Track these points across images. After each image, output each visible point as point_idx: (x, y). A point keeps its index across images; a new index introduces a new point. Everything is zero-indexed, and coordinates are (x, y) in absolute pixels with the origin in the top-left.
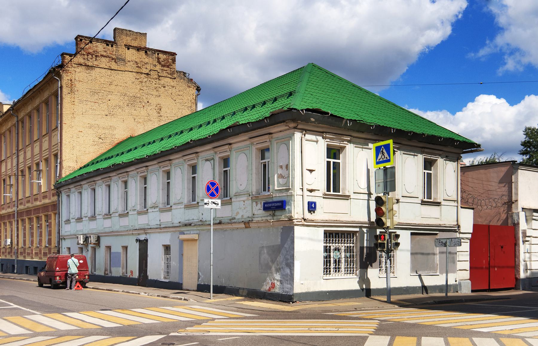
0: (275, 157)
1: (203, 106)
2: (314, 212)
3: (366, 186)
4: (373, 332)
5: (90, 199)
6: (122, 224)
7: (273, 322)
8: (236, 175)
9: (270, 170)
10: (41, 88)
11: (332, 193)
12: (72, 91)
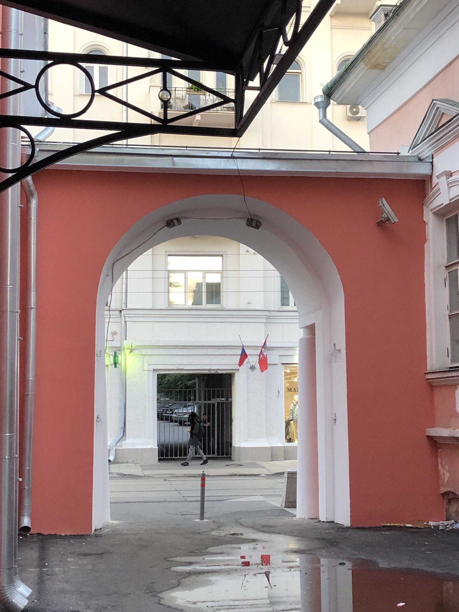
0: (447, 28)
1: (376, 26)
2: (248, 225)
3: (129, 102)
4: (180, 581)
5: (177, 372)
6: (216, 263)
8: (123, 145)
9: (253, 324)
10: (263, 606)
11: (220, 456)
12: (442, 204)
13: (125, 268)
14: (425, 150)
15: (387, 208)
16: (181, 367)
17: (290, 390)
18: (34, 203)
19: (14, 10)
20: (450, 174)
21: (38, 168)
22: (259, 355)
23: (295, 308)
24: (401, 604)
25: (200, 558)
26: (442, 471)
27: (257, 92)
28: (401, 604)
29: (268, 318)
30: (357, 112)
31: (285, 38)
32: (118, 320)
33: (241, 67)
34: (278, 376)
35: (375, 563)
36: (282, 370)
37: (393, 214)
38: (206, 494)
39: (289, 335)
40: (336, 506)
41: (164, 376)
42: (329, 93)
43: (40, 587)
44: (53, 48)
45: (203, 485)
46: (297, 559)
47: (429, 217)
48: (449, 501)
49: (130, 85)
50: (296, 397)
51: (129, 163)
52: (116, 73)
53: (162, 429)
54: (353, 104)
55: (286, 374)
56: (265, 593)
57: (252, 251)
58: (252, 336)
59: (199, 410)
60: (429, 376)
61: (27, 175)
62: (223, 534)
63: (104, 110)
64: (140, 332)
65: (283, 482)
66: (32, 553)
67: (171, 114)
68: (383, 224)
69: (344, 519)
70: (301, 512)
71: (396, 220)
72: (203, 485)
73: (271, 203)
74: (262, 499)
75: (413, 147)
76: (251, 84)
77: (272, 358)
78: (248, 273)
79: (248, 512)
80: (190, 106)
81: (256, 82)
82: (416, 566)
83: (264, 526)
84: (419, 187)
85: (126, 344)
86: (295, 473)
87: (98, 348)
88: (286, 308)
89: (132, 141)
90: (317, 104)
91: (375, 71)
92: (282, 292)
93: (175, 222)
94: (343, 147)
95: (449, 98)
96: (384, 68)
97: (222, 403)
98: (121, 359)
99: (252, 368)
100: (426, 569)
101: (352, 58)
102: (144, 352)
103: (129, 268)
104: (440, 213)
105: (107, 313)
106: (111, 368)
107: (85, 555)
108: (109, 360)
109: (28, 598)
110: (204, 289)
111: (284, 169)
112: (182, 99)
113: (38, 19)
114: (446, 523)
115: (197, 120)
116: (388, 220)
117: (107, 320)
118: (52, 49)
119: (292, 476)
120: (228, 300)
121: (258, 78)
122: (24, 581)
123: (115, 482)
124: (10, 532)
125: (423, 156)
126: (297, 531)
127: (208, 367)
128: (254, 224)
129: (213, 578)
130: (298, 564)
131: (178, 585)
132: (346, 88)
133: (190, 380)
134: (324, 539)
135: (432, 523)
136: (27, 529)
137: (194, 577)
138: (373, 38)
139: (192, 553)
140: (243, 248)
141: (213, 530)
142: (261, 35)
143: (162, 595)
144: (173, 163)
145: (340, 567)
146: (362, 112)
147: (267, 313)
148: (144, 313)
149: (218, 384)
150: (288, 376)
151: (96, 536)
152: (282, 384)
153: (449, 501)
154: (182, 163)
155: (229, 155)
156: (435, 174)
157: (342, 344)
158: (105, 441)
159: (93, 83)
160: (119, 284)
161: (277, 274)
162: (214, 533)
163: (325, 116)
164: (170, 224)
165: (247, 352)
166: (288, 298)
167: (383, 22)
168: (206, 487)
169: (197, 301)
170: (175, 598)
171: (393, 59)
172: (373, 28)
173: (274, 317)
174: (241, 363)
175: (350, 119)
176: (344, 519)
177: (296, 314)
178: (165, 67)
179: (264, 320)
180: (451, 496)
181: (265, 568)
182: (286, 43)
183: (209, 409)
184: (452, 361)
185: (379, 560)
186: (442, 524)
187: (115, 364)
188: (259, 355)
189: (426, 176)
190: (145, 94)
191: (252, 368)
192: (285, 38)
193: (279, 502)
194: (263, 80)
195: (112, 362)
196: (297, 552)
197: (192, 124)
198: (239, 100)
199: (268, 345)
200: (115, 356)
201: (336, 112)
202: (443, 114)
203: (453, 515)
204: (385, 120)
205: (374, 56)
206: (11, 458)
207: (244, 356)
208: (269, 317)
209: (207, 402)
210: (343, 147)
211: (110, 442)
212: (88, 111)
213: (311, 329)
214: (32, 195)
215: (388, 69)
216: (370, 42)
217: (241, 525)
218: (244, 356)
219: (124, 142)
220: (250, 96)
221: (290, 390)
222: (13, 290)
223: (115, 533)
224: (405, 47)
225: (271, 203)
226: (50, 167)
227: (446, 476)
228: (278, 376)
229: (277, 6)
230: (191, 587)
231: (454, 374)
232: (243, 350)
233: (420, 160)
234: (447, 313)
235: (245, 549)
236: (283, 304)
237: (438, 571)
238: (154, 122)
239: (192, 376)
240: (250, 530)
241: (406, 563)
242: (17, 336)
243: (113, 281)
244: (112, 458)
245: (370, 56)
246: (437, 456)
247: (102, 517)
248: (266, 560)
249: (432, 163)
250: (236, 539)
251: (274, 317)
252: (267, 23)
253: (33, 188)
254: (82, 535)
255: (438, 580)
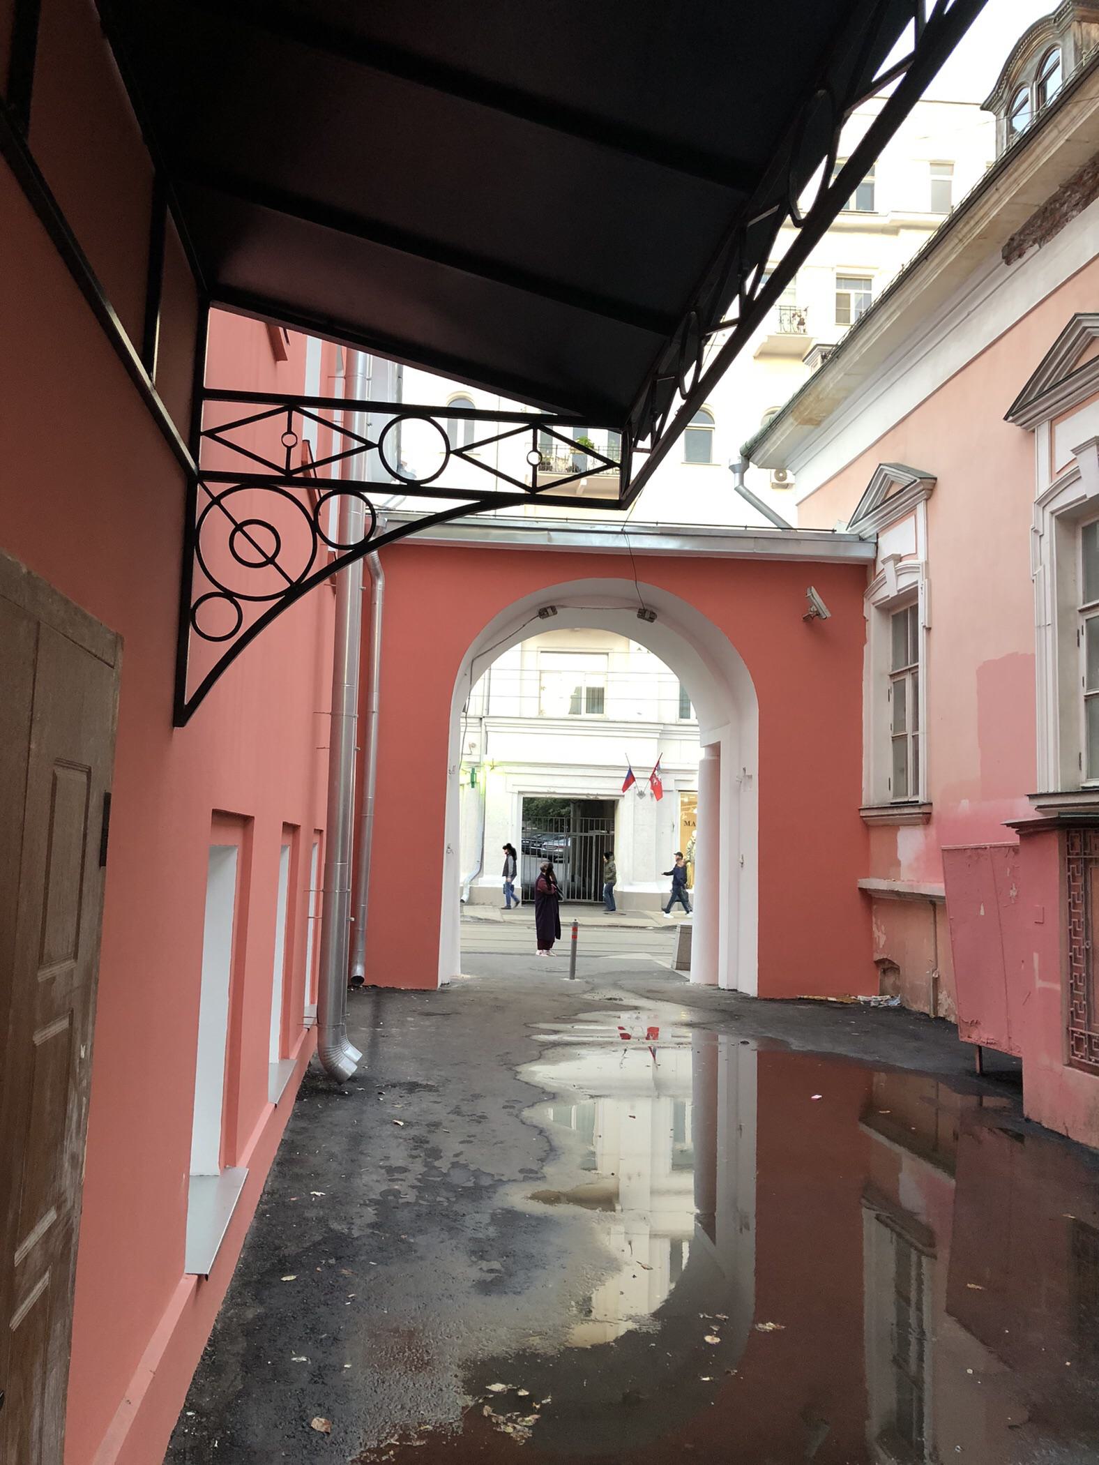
4: (542, 1052)
7: (1019, 166)
13: (487, 665)
14: (867, 528)
15: (817, 599)
16: (552, 790)
17: (688, 823)
18: (380, 584)
19: (361, 354)
20: (899, 559)
21: (387, 542)
22: (651, 779)
23: (696, 722)
24: (817, 1097)
25: (569, 1026)
26: (877, 933)
27: (648, 455)
28: (817, 1097)
29: (663, 733)
30: (784, 478)
31: (682, 390)
32: (478, 729)
33: (630, 423)
34: (673, 805)
35: (786, 1044)
36: (678, 799)
37: (823, 607)
38: (578, 947)
39: (687, 755)
40: (740, 971)
41: (532, 799)
42: (748, 454)
43: (372, 1050)
44: (408, 399)
45: (575, 937)
46: (689, 1034)
47: (870, 612)
48: (884, 972)
49: (500, 441)
50: (695, 833)
51: (495, 537)
52: (484, 429)
53: (527, 865)
54: (780, 467)
55: (682, 803)
56: (648, 1074)
57: (644, 649)
58: (642, 754)
59: (572, 842)
60: (863, 814)
61: (372, 549)
62: (597, 998)
63: (461, 476)
64: (504, 745)
65: (675, 937)
66: (363, 1010)
67: (544, 478)
68: (811, 620)
69: (750, 987)
70: (696, 976)
71: (828, 614)
72: (575, 937)
73: (678, 591)
74: (648, 957)
75: (853, 523)
76: (641, 444)
77: (668, 783)
78: (638, 676)
79: (629, 972)
80: (574, 468)
81: (646, 443)
82: (841, 1050)
83: (649, 991)
84: (859, 574)
85: (487, 760)
86: (690, 928)
87: (451, 764)
88: (685, 721)
89: (500, 511)
90: (732, 468)
91: (808, 427)
92: (682, 701)
93: (549, 611)
94: (765, 522)
95: (900, 462)
96: (818, 423)
97: (602, 837)
98: (479, 777)
99: (641, 794)
100: (852, 1055)
101: (779, 410)
102: (508, 769)
103: (493, 666)
104: (886, 608)
105: (463, 720)
106: (468, 788)
107: (428, 1014)
108: (464, 778)
109: (357, 1063)
110: (584, 695)
111: (687, 548)
112: (565, 460)
113: (391, 366)
114: (879, 998)
115: (582, 487)
116: (818, 614)
117: (463, 729)
118: (406, 400)
119: (686, 931)
120: (612, 708)
121: (649, 437)
122: (353, 1042)
123: (467, 928)
124: (338, 981)
125: (865, 535)
126: (690, 1000)
127: (586, 792)
128: (647, 616)
129: (583, 1051)
130: (690, 1040)
131: (539, 1058)
132: (771, 447)
133: (564, 807)
134: (723, 1011)
135: (861, 998)
136: (360, 979)
137: (559, 1049)
138: (806, 386)
139: (565, 1021)
140: (634, 645)
141: (585, 992)
142: (654, 384)
143: (519, 1069)
144: (550, 539)
145: (742, 1047)
146: (790, 478)
147: (661, 727)
148: (519, 722)
149: (595, 816)
150: (686, 806)
151: (443, 992)
152: (678, 816)
153: (884, 972)
154: (560, 540)
155: (619, 529)
156: (881, 558)
157: (754, 769)
158: (456, 877)
159: (448, 440)
160: (479, 687)
161: (675, 678)
162: (587, 996)
163: (742, 482)
164: (543, 613)
165: (635, 774)
166: (689, 709)
167: (819, 366)
168: (579, 939)
169: (575, 710)
170: (534, 1073)
171: (830, 412)
172: (802, 373)
173: (670, 733)
174: (626, 786)
175: (775, 486)
176: (750, 987)
177: (698, 729)
178: (534, 423)
179: (658, 736)
180: (887, 965)
181: (650, 1043)
182: (683, 397)
183: (586, 842)
184: (895, 795)
185: (791, 1040)
186: (874, 999)
187: (473, 783)
188: (651, 779)
189: (868, 560)
190: (514, 456)
191: (641, 794)
192: (682, 390)
193: (668, 963)
194: (655, 442)
195: (469, 780)
196: (689, 1025)
197: (575, 492)
198: (625, 466)
199: (662, 766)
200: (473, 773)
201: (759, 478)
202: (892, 482)
203: (890, 990)
204: (818, 489)
205: (806, 409)
206: (342, 894)
207: (630, 779)
208: (664, 732)
209: (584, 834)
210: (765, 522)
211: (464, 877)
212: (441, 476)
213: (715, 749)
214: (378, 575)
215: (823, 425)
216: (802, 391)
217: (621, 988)
218: (630, 779)
219: (492, 512)
220: (639, 461)
221: (688, 823)
222: (350, 690)
223: (466, 989)
224: (846, 398)
225: (678, 591)
226: (396, 542)
227: (881, 937)
228: (673, 805)
229: (674, 349)
230: (554, 1061)
231: (896, 812)
232: (630, 772)
233: (862, 540)
234: (891, 734)
235: (625, 1017)
236: (682, 717)
237: (866, 1057)
238: (522, 491)
239: (566, 802)
240: (632, 995)
241: (826, 1046)
242: (354, 745)
243: (472, 682)
244: (465, 898)
245: (802, 409)
246: (871, 912)
247: (450, 969)
248: (653, 1033)
249: (876, 544)
250: (614, 1006)
251: (670, 733)
252: (662, 370)
253: (379, 566)
254: (427, 991)
255: (871, 1068)
